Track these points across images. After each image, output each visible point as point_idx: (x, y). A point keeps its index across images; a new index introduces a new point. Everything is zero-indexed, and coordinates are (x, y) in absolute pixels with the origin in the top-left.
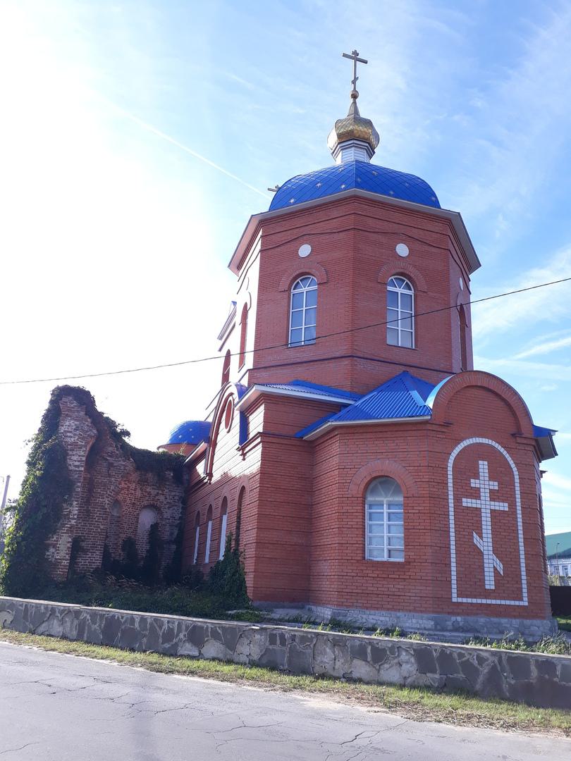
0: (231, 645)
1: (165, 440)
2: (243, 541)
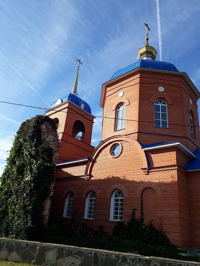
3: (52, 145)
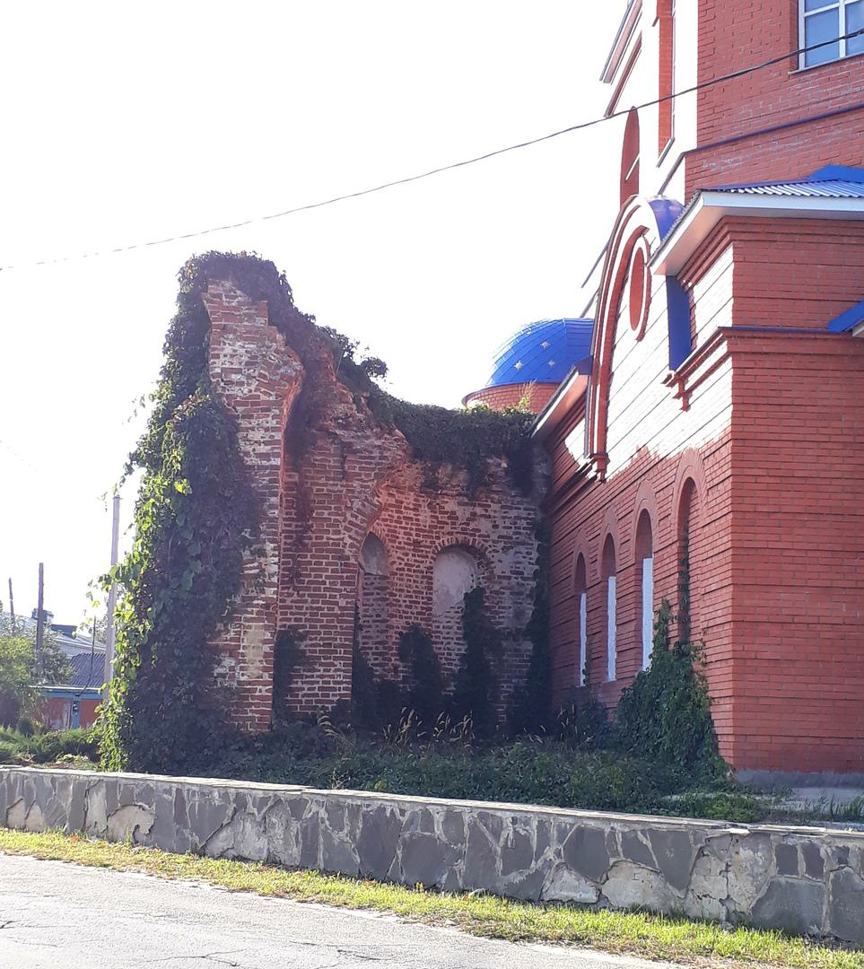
0: (678, 876)
1: (480, 375)
2: (699, 622)
3: (242, 384)
